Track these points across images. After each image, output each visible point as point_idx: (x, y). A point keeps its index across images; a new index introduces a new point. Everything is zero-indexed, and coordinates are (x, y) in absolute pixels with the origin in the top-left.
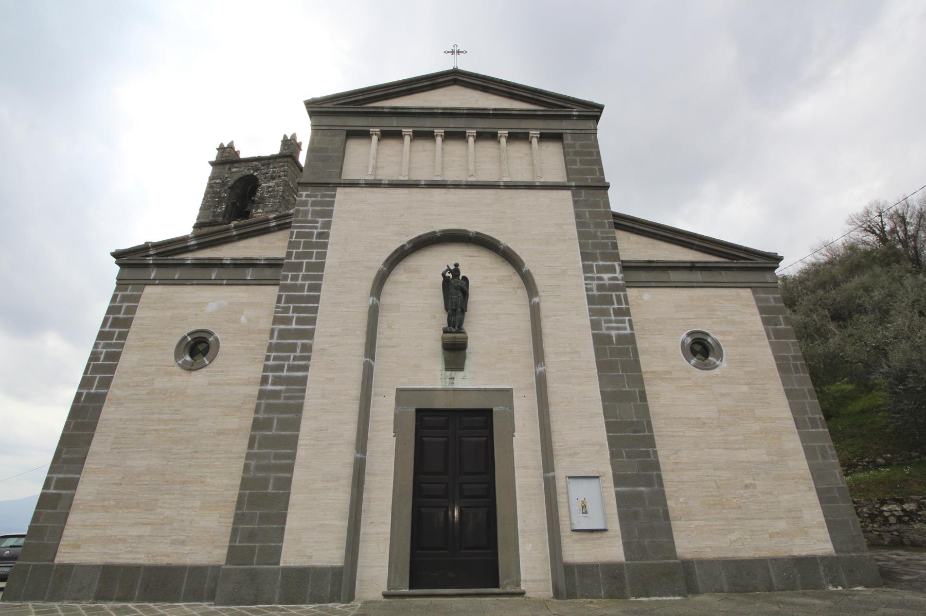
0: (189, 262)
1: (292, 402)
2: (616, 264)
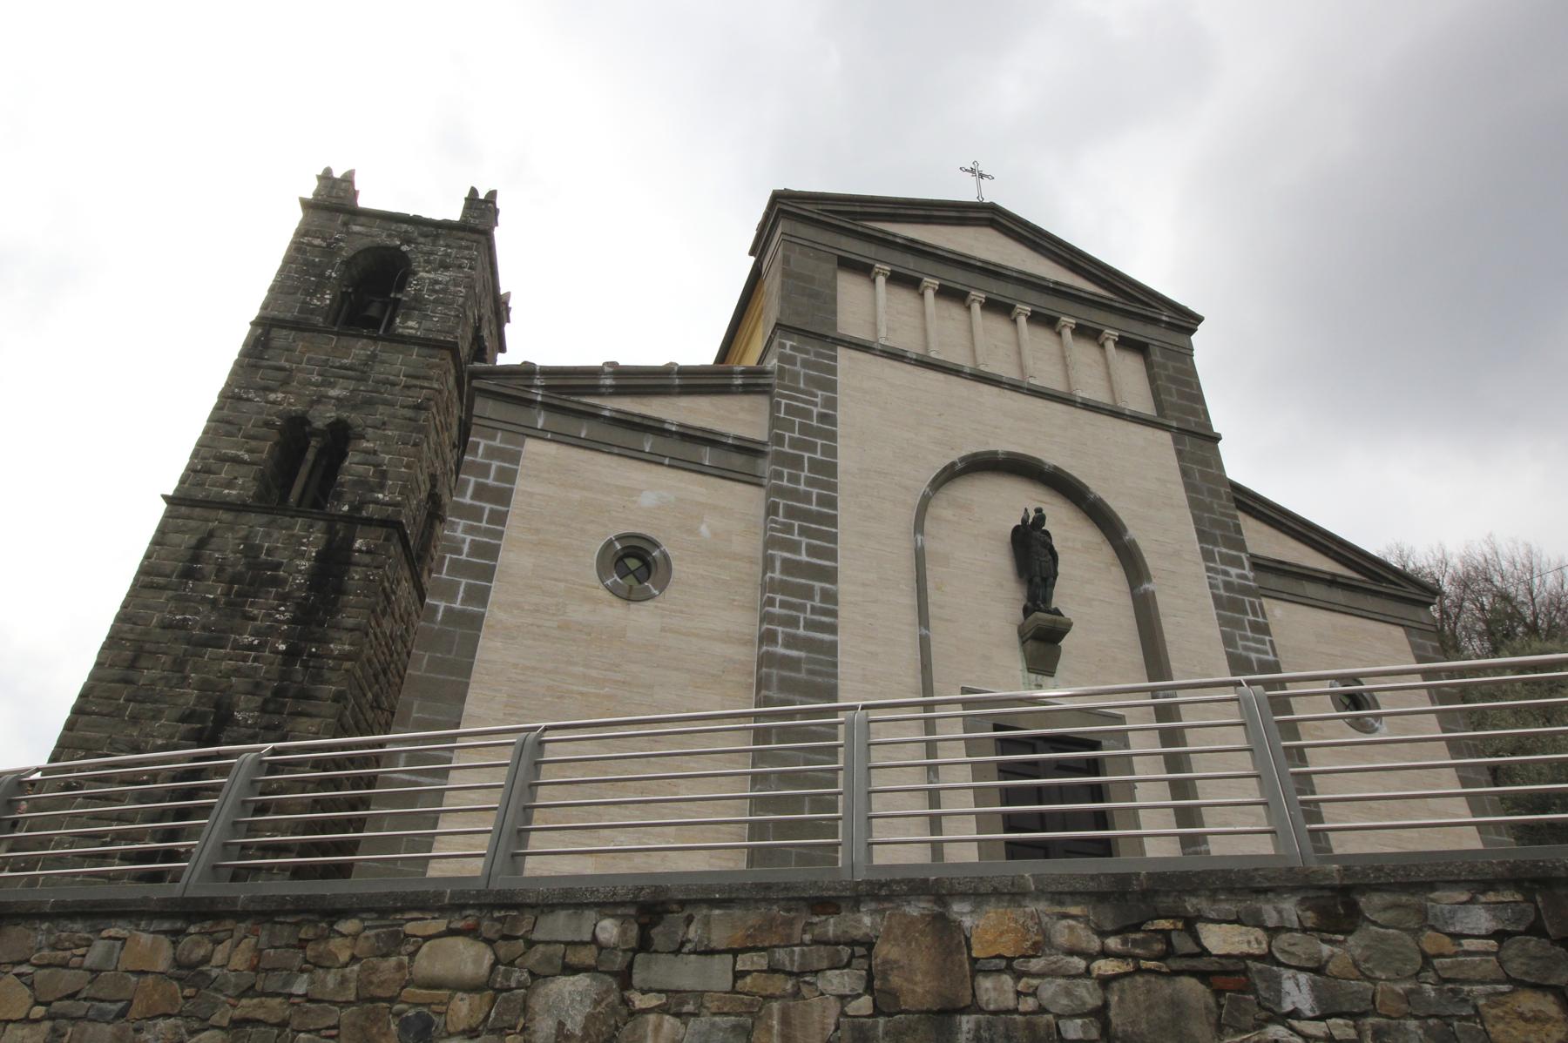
0: (606, 413)
1: (820, 679)
2: (1243, 555)
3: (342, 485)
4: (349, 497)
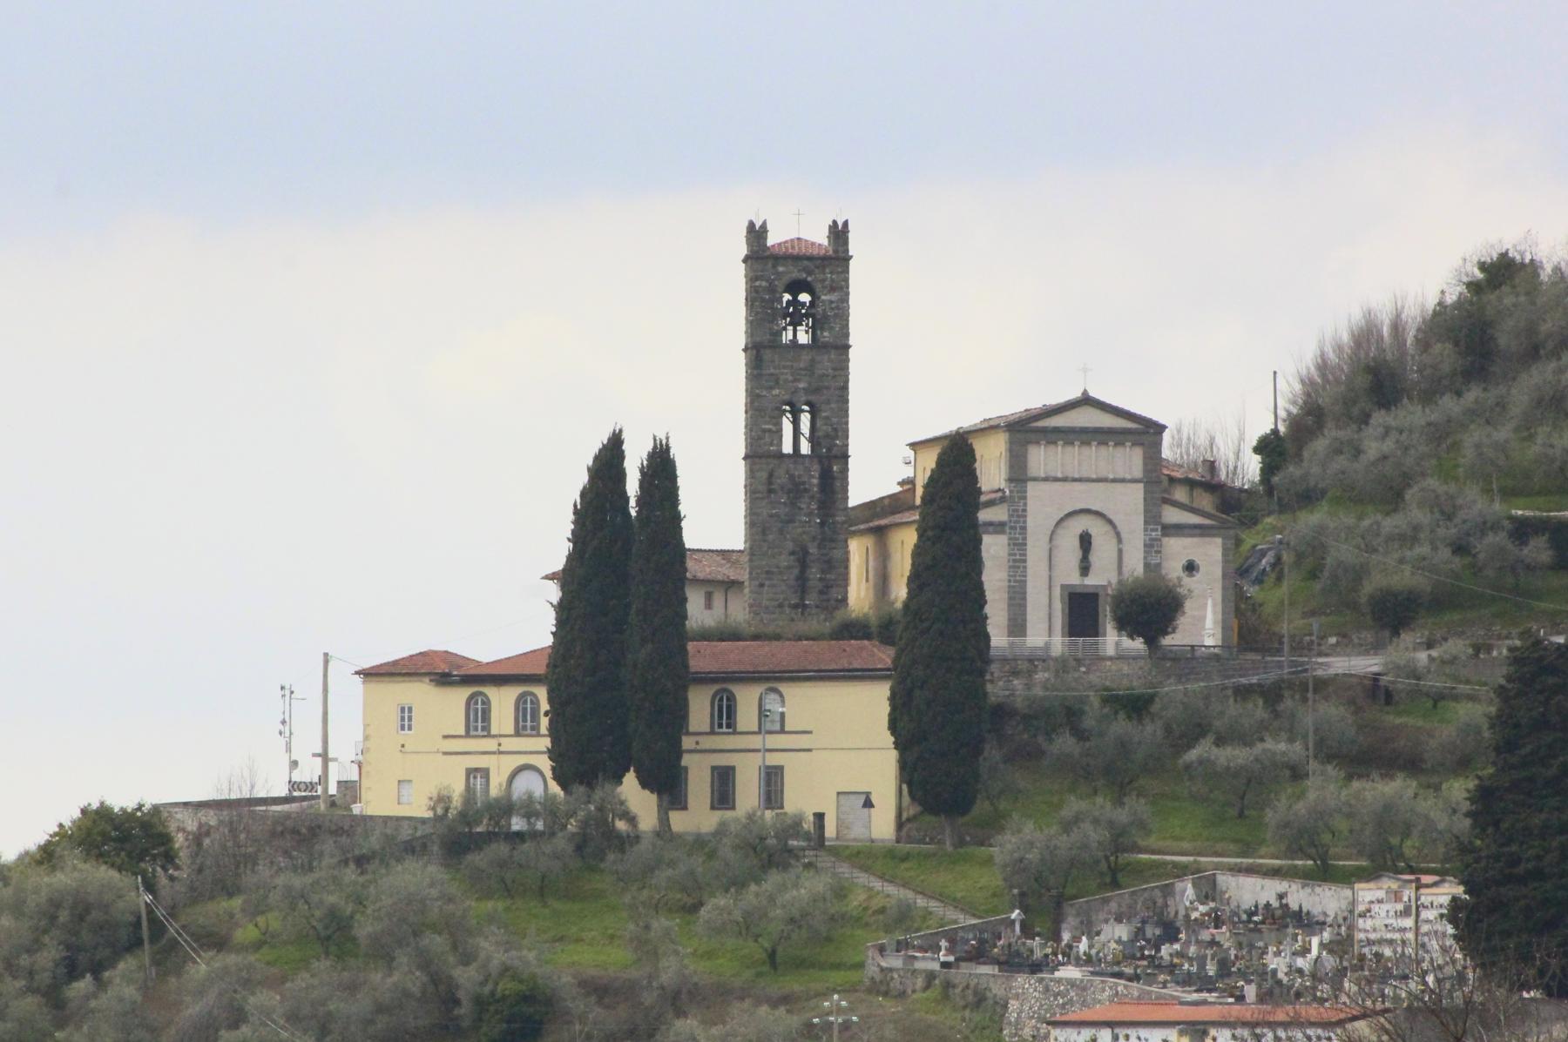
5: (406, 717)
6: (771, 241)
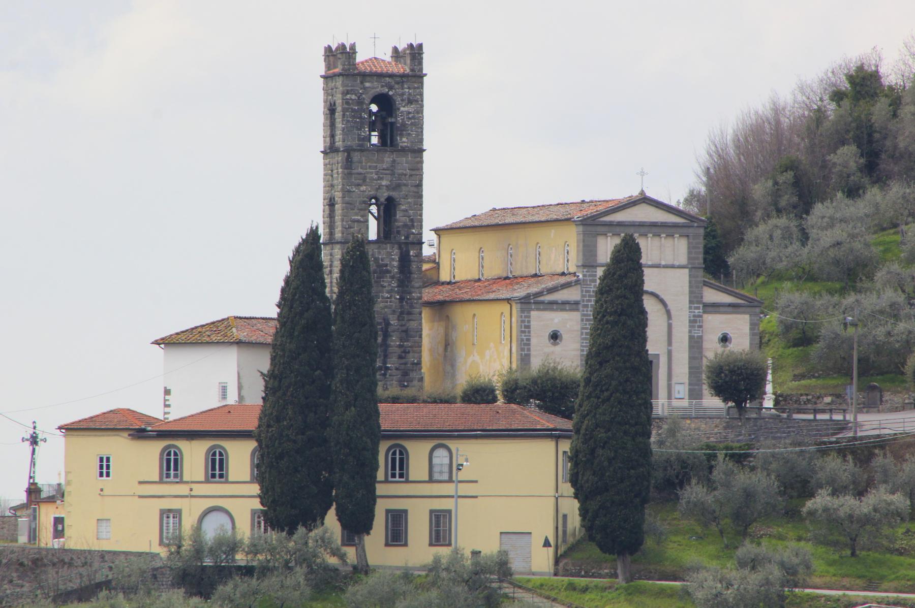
3: (398, 227)
4: (402, 232)
5: (104, 467)
6: (359, 58)
